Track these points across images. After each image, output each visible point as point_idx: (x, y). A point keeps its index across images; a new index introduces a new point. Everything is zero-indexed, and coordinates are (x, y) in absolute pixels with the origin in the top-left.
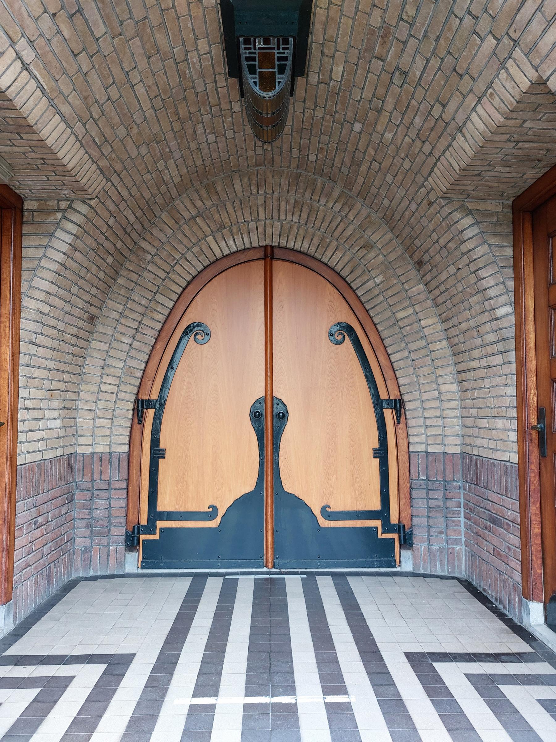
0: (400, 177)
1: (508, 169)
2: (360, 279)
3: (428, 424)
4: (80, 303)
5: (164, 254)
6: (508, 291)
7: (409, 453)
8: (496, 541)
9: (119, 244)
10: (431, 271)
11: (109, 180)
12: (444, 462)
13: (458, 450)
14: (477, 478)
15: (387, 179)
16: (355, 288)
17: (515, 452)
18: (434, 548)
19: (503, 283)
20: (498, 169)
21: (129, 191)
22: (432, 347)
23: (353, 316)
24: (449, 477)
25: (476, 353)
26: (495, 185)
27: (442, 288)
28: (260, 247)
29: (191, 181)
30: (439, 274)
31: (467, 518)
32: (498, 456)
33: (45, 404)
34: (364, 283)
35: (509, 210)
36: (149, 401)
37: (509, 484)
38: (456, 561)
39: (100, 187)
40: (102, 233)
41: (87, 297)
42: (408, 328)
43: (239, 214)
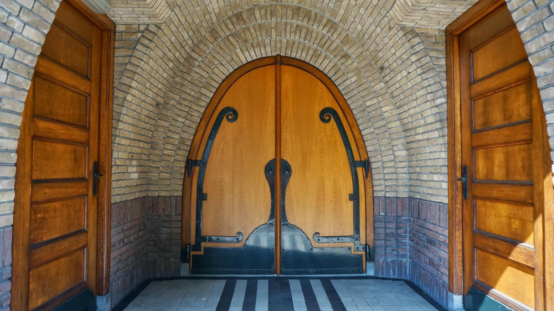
0: (370, 10)
1: (444, 6)
2: (341, 78)
3: (386, 178)
4: (151, 94)
5: (206, 61)
6: (443, 88)
7: (373, 198)
8: (431, 255)
9: (177, 54)
10: (389, 74)
11: (173, 11)
12: (397, 203)
13: (405, 195)
14: (419, 214)
15: (361, 11)
16: (337, 85)
17: (446, 196)
18: (389, 260)
19: (439, 83)
20: (437, 6)
21: (185, 18)
22: (390, 125)
23: (336, 104)
24: (400, 213)
25: (420, 130)
26: (435, 16)
27: (398, 85)
28: (272, 56)
29: (226, 12)
30: (395, 76)
31: (411, 240)
32: (433, 199)
33: (128, 163)
34: (344, 81)
35: (443, 34)
36: (196, 161)
37: (441, 217)
38: (403, 269)
39: (167, 16)
40: (167, 47)
41: (155, 90)
42: (374, 112)
43: (259, 33)
